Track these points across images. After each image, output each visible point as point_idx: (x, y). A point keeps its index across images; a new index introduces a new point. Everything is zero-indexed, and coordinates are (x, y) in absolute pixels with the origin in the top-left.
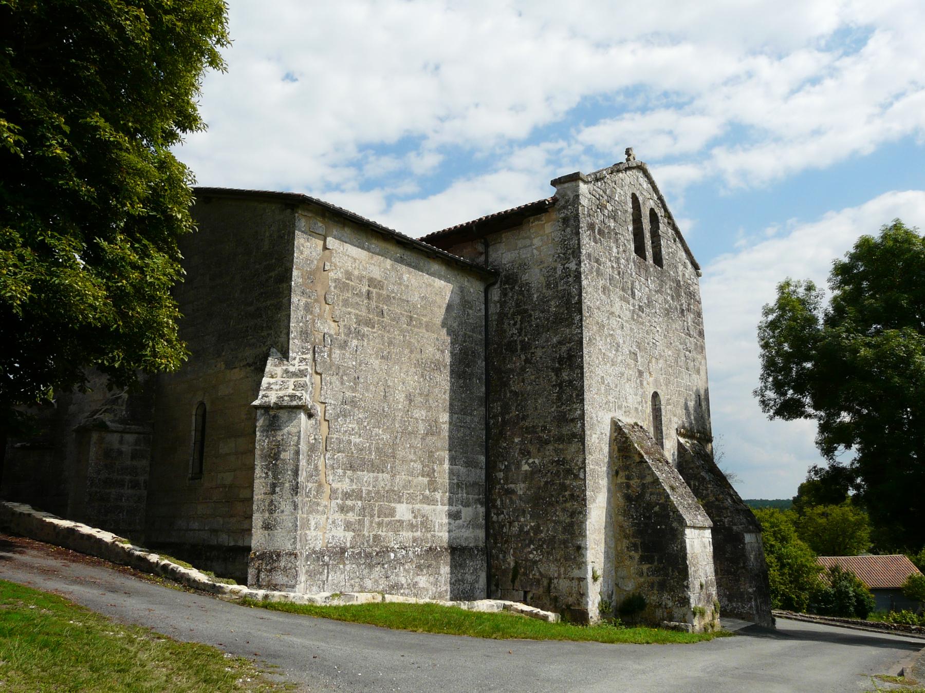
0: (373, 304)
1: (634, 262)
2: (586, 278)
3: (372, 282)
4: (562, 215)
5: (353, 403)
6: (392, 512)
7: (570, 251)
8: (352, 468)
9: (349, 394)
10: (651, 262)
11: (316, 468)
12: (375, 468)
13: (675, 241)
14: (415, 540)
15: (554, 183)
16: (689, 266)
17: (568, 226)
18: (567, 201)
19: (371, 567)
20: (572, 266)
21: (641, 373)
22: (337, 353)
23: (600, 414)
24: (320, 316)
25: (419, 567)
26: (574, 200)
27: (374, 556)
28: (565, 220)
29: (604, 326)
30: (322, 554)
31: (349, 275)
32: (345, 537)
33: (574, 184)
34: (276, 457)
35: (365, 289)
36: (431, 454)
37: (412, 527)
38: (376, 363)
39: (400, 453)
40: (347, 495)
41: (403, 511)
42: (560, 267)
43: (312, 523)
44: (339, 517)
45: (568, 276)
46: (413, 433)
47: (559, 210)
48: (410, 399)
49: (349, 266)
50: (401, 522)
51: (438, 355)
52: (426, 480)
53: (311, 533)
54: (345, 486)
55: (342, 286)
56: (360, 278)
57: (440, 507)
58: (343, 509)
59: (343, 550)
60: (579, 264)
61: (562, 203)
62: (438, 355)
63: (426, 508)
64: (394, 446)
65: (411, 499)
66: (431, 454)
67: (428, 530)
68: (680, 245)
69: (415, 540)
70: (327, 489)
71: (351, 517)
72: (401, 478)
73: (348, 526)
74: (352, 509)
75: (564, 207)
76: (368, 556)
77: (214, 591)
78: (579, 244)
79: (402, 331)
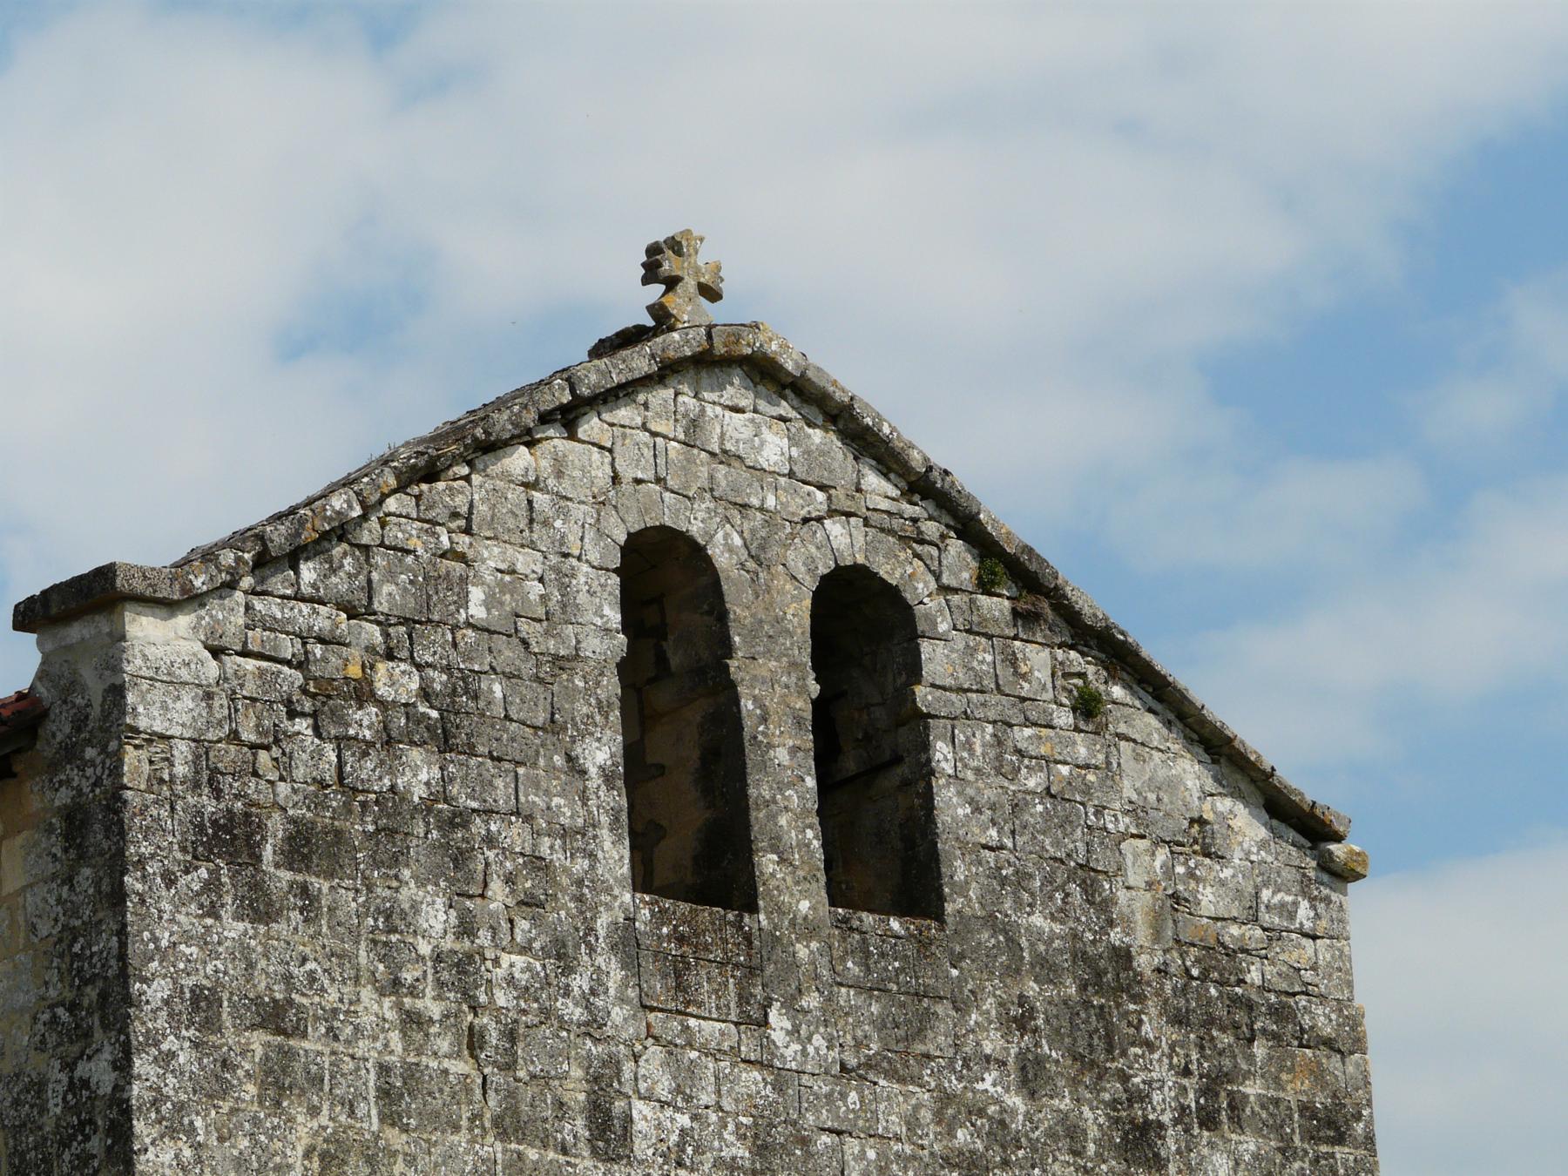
1: (627, 943)
2: (174, 1129)
4: (63, 797)
7: (92, 993)
10: (808, 903)
13: (1088, 707)
15: (30, 616)
16: (1246, 827)
17: (82, 857)
18: (80, 723)
20: (99, 1070)
26: (106, 715)
28: (74, 822)
33: (103, 624)
42: (57, 1077)
45: (85, 1127)
47: (54, 767)
60: (123, 1066)
61: (59, 728)
68: (1148, 725)
75: (71, 753)
78: (122, 957)
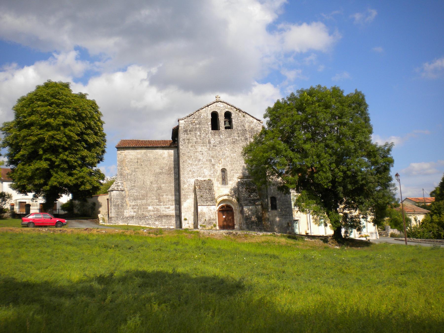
0: (139, 164)
3: (138, 159)
5: (134, 186)
6: (147, 208)
8: (135, 200)
9: (133, 185)
10: (224, 129)
11: (126, 201)
12: (141, 199)
13: (244, 116)
14: (154, 214)
16: (255, 121)
19: (141, 220)
21: (213, 165)
22: (129, 177)
23: (188, 180)
24: (125, 170)
25: (156, 220)
27: (142, 217)
29: (191, 156)
30: (128, 217)
31: (131, 159)
32: (133, 214)
34: (111, 200)
35: (136, 161)
36: (159, 195)
37: (153, 211)
38: (140, 177)
39: (149, 195)
40: (134, 206)
41: (150, 208)
43: (125, 212)
44: (132, 210)
46: (153, 190)
48: (151, 183)
49: (131, 157)
50: (150, 210)
51: (160, 171)
52: (157, 201)
53: (125, 214)
54: (133, 204)
55: (129, 162)
56: (135, 159)
57: (162, 206)
58: (132, 208)
59: (133, 217)
62: (160, 171)
63: (158, 207)
64: (147, 194)
65: (153, 205)
66: (159, 195)
67: (158, 212)
69: (154, 214)
70: (129, 205)
71: (135, 210)
72: (149, 201)
73: (134, 212)
74: (135, 208)
76: (141, 218)
77: (246, 237)
79: (148, 167)
